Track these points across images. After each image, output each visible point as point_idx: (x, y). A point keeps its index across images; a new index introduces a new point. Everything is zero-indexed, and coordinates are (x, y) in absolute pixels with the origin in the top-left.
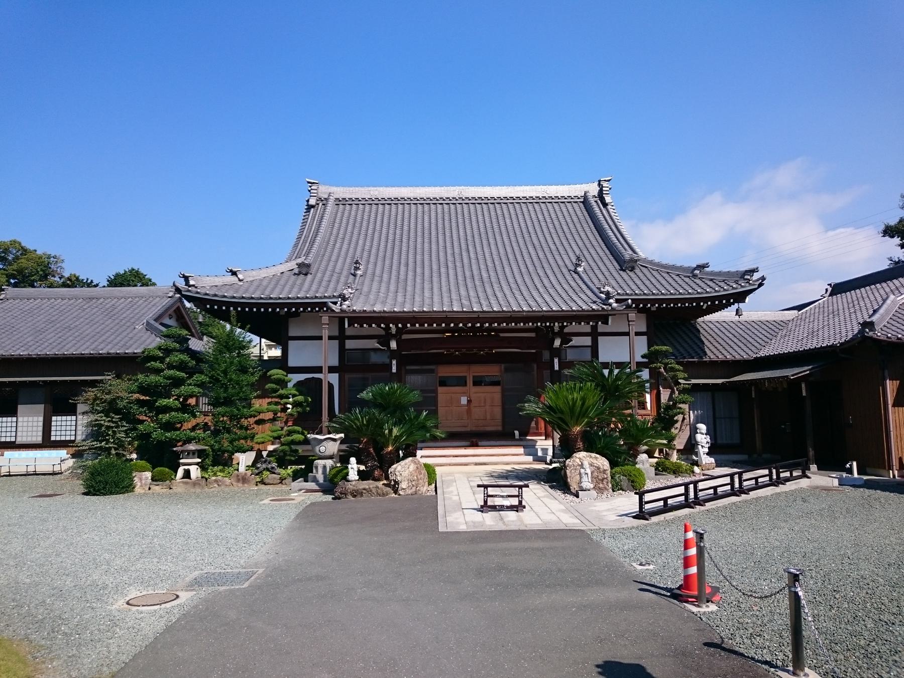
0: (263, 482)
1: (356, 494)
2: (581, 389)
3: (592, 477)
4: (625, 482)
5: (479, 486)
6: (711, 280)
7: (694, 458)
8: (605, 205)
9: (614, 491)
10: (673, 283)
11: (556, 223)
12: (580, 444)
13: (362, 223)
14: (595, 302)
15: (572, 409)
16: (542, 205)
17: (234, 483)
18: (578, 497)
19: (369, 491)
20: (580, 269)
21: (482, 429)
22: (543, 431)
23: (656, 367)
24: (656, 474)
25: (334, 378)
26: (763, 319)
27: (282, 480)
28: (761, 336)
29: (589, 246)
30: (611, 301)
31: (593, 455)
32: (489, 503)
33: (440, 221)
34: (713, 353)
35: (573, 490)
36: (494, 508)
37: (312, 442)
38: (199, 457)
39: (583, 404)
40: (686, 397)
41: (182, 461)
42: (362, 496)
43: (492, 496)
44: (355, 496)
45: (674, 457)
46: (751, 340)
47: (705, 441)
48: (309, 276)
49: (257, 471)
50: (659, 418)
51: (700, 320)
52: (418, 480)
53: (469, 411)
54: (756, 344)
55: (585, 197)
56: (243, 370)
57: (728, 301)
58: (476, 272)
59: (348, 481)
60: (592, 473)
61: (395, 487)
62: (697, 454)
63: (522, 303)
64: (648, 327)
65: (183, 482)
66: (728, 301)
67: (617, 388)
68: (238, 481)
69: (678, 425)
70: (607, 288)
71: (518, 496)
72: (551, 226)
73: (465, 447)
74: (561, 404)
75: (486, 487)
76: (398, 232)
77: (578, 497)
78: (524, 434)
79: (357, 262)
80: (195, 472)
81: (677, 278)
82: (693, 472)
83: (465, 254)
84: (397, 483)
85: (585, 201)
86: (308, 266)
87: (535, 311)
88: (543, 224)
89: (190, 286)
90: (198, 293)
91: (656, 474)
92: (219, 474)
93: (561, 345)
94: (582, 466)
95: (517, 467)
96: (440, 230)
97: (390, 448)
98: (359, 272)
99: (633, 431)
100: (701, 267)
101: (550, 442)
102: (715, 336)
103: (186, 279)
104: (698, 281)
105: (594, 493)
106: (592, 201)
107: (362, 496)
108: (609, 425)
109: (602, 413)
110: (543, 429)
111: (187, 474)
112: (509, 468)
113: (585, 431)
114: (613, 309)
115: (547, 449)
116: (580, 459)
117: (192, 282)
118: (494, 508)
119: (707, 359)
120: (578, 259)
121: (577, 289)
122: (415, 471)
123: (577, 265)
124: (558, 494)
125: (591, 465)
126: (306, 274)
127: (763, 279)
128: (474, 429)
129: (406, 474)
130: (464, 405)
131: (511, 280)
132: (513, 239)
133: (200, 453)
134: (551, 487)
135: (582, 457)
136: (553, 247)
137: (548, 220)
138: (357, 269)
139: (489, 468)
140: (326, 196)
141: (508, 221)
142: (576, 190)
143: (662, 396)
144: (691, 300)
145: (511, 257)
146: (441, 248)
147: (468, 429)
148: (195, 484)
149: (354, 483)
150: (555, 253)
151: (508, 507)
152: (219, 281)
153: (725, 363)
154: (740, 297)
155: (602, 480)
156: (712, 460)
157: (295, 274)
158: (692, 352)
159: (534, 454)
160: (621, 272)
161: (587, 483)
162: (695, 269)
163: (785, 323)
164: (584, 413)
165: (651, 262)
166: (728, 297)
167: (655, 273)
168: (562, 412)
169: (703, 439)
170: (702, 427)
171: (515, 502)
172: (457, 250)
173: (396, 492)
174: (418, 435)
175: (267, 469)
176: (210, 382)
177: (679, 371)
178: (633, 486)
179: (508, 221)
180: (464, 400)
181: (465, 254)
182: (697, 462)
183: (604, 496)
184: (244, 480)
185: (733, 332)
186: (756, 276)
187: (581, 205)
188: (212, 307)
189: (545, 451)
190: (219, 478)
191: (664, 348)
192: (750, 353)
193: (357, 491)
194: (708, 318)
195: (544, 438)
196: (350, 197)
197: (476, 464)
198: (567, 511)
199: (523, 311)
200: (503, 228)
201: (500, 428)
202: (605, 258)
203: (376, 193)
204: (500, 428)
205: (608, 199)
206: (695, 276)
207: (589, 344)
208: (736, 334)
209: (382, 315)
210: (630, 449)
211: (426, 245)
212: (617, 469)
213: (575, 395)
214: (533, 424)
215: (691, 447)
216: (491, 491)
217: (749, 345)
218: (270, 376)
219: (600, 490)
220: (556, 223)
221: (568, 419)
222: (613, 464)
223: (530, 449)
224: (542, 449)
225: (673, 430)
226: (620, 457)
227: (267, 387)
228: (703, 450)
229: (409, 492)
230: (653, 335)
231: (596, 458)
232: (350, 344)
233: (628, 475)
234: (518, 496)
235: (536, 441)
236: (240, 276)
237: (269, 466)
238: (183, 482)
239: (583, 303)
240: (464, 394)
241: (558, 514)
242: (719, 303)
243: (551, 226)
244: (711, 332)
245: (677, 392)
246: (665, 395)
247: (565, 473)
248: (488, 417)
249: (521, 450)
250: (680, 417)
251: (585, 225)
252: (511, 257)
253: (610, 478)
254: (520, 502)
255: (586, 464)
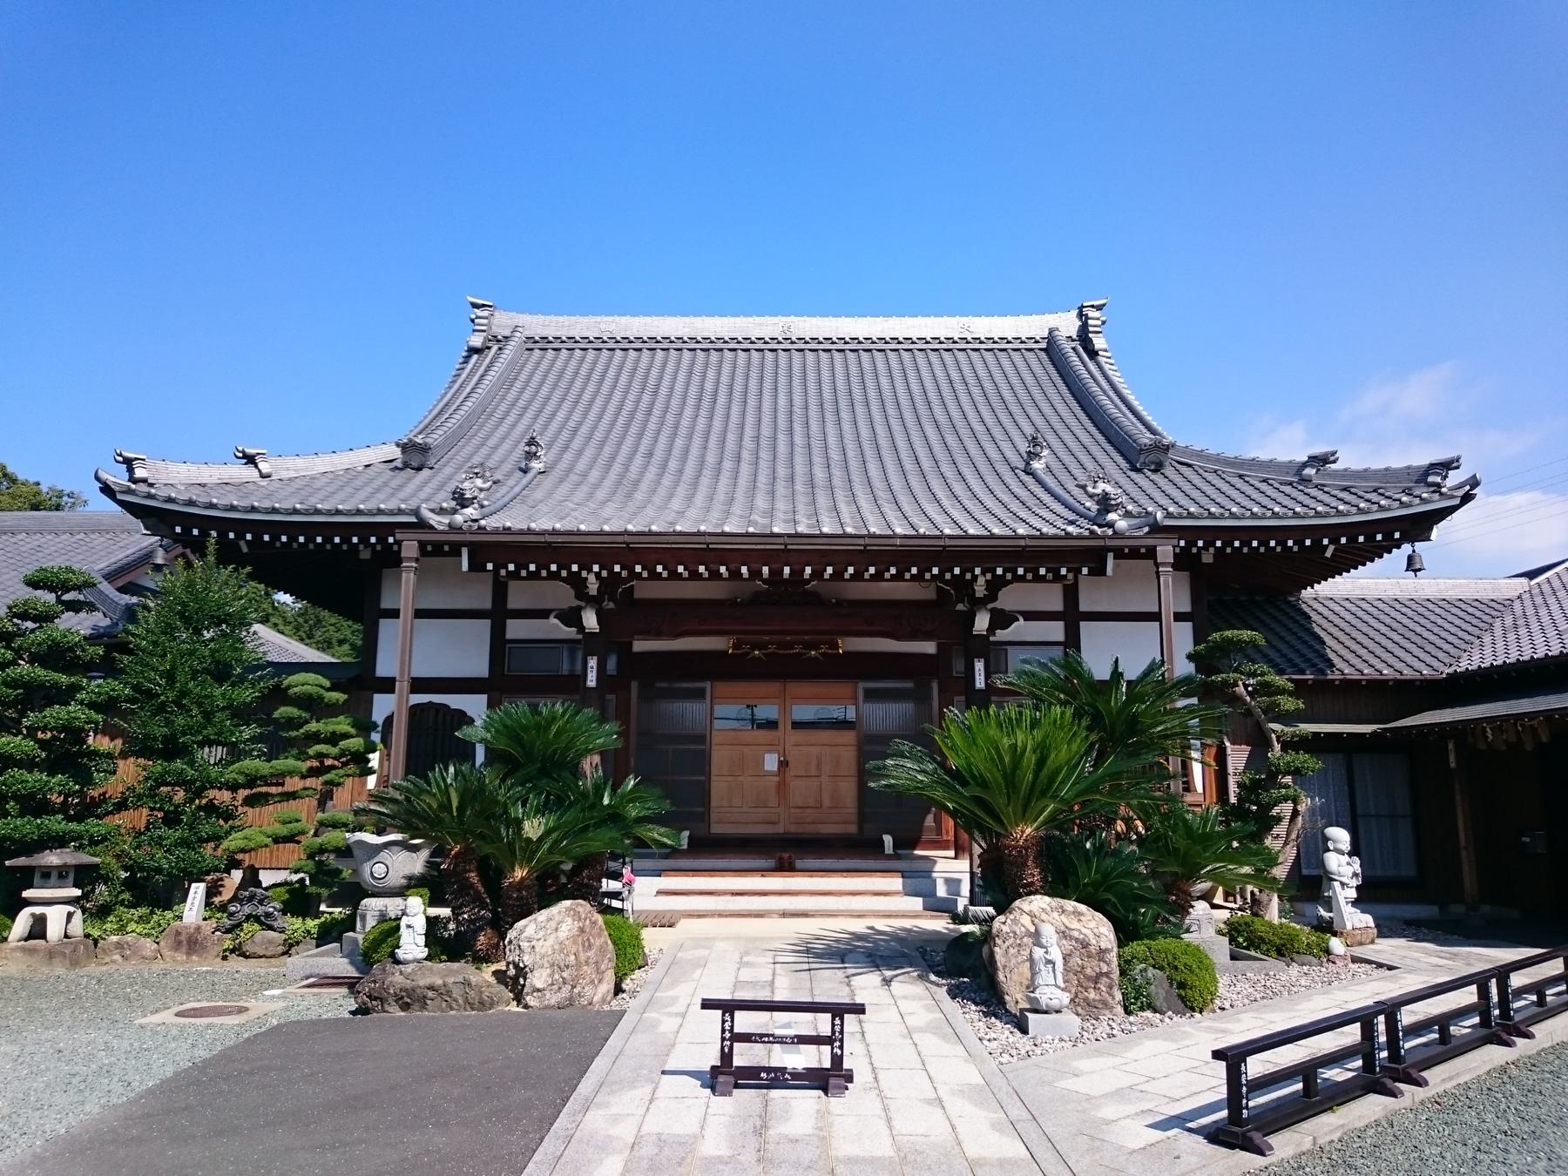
0: (238, 951)
1: (409, 1000)
2: (1035, 724)
3: (1067, 970)
4: (1159, 988)
5: (707, 1005)
6: (1345, 489)
7: (1322, 912)
8: (1093, 354)
9: (1128, 1012)
10: (1255, 495)
11: (988, 385)
12: (1033, 874)
13: (572, 382)
14: (1072, 523)
15: (1011, 778)
16: (960, 355)
17: (167, 953)
18: (1024, 1031)
19: (443, 992)
20: (1037, 465)
21: (810, 829)
22: (951, 837)
23: (1225, 683)
24: (1233, 958)
25: (474, 705)
26: (1451, 594)
27: (289, 947)
28: (1453, 630)
29: (1058, 426)
30: (1112, 516)
31: (1070, 905)
32: (738, 1061)
33: (739, 380)
34: (1347, 664)
35: (1011, 1007)
36: (752, 1077)
37: (356, 852)
38: (75, 886)
39: (1041, 763)
40: (1302, 758)
41: (25, 894)
42: (424, 1006)
43: (746, 1038)
44: (405, 1007)
45: (1273, 912)
46: (1432, 638)
47: (1348, 871)
48: (425, 473)
49: (227, 922)
50: (1233, 813)
51: (1307, 593)
52: (578, 965)
53: (782, 787)
54: (1446, 647)
55: (1051, 339)
56: (221, 673)
57: (1388, 536)
58: (800, 469)
59: (398, 962)
60: (1066, 958)
61: (515, 981)
62: (1329, 904)
63: (892, 515)
64: (1194, 602)
65: (23, 949)
66: (1388, 536)
67: (1133, 725)
68: (177, 945)
69: (1280, 829)
70: (1102, 487)
71: (828, 1041)
72: (976, 391)
73: (763, 872)
74: (981, 765)
75: (729, 1007)
76: (646, 398)
77: (1024, 1031)
78: (907, 842)
79: (532, 442)
80: (56, 918)
81: (1264, 487)
82: (1328, 952)
83: (782, 439)
84: (521, 972)
85: (1051, 347)
86: (424, 449)
87: (925, 537)
88: (959, 387)
89: (135, 481)
90: (150, 496)
91: (1233, 958)
92: (132, 926)
93: (992, 629)
94: (1036, 936)
95: (881, 925)
96: (737, 395)
97: (519, 873)
98: (536, 465)
99: (1178, 840)
100: (1321, 461)
101: (963, 865)
102: (1348, 629)
103: (129, 463)
104: (1314, 492)
105: (1071, 1021)
106: (1067, 347)
107: (424, 1006)
108: (1110, 822)
109: (1093, 788)
110: (952, 833)
111: (38, 929)
112: (859, 926)
113: (1047, 839)
114: (1117, 535)
115: (959, 881)
116: (1032, 915)
117: (139, 473)
118: (752, 1077)
119: (1337, 676)
120: (1034, 441)
121: (1031, 502)
122: (574, 939)
123: (1033, 455)
124: (967, 1016)
125: (1064, 934)
126: (419, 469)
127: (1474, 482)
128: (793, 829)
129: (545, 947)
130: (770, 774)
131: (878, 484)
132: (891, 411)
133: (84, 876)
134: (954, 993)
135: (1036, 906)
136: (978, 427)
137: (971, 381)
138: (531, 456)
139: (811, 927)
140: (507, 333)
141: (884, 381)
142: (1033, 326)
143: (1230, 761)
144: (1299, 532)
145: (884, 442)
146: (732, 426)
147: (780, 829)
148: (51, 954)
149: (409, 969)
150: (984, 438)
151: (796, 1075)
152: (211, 474)
153: (1377, 687)
154: (1418, 526)
155: (1096, 979)
156: (1368, 920)
157: (396, 468)
158: (1298, 661)
159: (928, 894)
160: (1133, 475)
161: (1051, 992)
162: (1304, 465)
163: (1508, 604)
164: (1043, 788)
165: (1200, 455)
166: (1387, 525)
167: (1210, 477)
168: (983, 784)
169: (1343, 867)
170: (1340, 836)
171: (817, 1057)
172: (766, 431)
173: (519, 998)
174: (598, 841)
175: (257, 919)
176: (133, 701)
177: (1282, 691)
178: (1183, 999)
179: (884, 381)
180: (771, 762)
181: (782, 439)
182: (1331, 922)
183: (1102, 1029)
184: (192, 944)
185: (1388, 620)
186: (1454, 478)
187: (1043, 355)
188: (187, 531)
189: (953, 884)
190: (129, 938)
191: (1246, 634)
192: (1436, 664)
193: (410, 992)
194: (1326, 588)
195: (952, 853)
196: (558, 334)
197: (785, 914)
198: (985, 1094)
199: (895, 536)
200: (872, 394)
201: (852, 829)
202: (1095, 450)
203: (613, 327)
204: (852, 829)
205: (1099, 342)
206: (1305, 481)
207: (1060, 637)
208: (1395, 625)
209: (549, 539)
210: (1168, 889)
211: (701, 422)
212: (1137, 947)
213: (1020, 737)
214: (929, 821)
215: (1309, 885)
216: (745, 1021)
217: (1429, 648)
218: (289, 687)
219: (1088, 1009)
220: (988, 385)
221: (999, 801)
222: (1126, 932)
223: (919, 881)
224: (948, 881)
225: (1268, 842)
226: (1140, 905)
227: (276, 715)
228: (1344, 893)
229: (553, 999)
230: (1206, 613)
231: (1078, 914)
232: (516, 629)
233: (1170, 966)
234: (828, 1041)
235: (931, 861)
236: (264, 467)
237: (261, 910)
238: (23, 949)
239: (1043, 521)
240: (771, 747)
241: (956, 1105)
242: (1361, 543)
243: (976, 391)
244: (1337, 621)
245: (1277, 747)
246: (1237, 757)
247: (992, 954)
248: (827, 802)
249: (896, 883)
250: (1286, 809)
251: (1051, 391)
252: (884, 442)
253: (1116, 975)
254: (837, 1060)
255: (1051, 933)
